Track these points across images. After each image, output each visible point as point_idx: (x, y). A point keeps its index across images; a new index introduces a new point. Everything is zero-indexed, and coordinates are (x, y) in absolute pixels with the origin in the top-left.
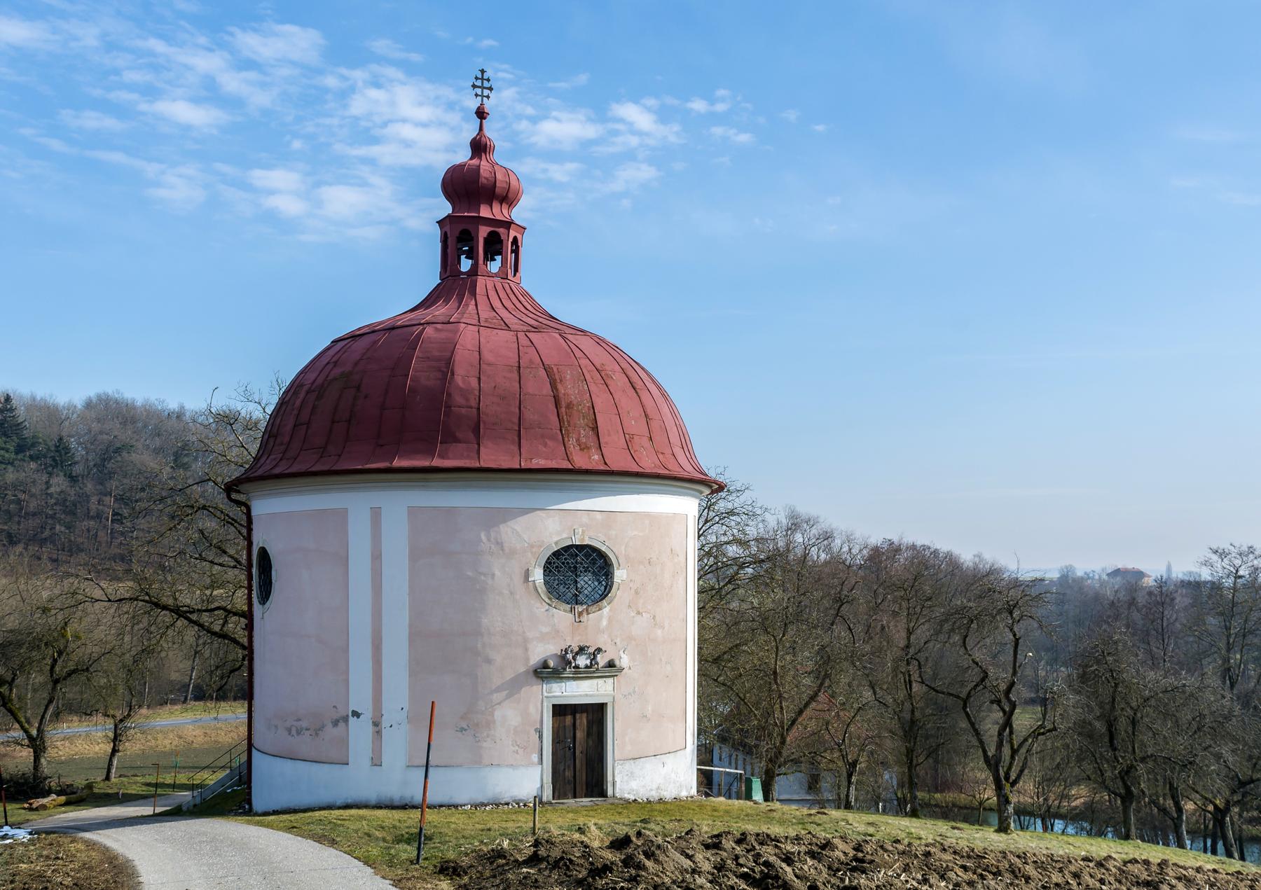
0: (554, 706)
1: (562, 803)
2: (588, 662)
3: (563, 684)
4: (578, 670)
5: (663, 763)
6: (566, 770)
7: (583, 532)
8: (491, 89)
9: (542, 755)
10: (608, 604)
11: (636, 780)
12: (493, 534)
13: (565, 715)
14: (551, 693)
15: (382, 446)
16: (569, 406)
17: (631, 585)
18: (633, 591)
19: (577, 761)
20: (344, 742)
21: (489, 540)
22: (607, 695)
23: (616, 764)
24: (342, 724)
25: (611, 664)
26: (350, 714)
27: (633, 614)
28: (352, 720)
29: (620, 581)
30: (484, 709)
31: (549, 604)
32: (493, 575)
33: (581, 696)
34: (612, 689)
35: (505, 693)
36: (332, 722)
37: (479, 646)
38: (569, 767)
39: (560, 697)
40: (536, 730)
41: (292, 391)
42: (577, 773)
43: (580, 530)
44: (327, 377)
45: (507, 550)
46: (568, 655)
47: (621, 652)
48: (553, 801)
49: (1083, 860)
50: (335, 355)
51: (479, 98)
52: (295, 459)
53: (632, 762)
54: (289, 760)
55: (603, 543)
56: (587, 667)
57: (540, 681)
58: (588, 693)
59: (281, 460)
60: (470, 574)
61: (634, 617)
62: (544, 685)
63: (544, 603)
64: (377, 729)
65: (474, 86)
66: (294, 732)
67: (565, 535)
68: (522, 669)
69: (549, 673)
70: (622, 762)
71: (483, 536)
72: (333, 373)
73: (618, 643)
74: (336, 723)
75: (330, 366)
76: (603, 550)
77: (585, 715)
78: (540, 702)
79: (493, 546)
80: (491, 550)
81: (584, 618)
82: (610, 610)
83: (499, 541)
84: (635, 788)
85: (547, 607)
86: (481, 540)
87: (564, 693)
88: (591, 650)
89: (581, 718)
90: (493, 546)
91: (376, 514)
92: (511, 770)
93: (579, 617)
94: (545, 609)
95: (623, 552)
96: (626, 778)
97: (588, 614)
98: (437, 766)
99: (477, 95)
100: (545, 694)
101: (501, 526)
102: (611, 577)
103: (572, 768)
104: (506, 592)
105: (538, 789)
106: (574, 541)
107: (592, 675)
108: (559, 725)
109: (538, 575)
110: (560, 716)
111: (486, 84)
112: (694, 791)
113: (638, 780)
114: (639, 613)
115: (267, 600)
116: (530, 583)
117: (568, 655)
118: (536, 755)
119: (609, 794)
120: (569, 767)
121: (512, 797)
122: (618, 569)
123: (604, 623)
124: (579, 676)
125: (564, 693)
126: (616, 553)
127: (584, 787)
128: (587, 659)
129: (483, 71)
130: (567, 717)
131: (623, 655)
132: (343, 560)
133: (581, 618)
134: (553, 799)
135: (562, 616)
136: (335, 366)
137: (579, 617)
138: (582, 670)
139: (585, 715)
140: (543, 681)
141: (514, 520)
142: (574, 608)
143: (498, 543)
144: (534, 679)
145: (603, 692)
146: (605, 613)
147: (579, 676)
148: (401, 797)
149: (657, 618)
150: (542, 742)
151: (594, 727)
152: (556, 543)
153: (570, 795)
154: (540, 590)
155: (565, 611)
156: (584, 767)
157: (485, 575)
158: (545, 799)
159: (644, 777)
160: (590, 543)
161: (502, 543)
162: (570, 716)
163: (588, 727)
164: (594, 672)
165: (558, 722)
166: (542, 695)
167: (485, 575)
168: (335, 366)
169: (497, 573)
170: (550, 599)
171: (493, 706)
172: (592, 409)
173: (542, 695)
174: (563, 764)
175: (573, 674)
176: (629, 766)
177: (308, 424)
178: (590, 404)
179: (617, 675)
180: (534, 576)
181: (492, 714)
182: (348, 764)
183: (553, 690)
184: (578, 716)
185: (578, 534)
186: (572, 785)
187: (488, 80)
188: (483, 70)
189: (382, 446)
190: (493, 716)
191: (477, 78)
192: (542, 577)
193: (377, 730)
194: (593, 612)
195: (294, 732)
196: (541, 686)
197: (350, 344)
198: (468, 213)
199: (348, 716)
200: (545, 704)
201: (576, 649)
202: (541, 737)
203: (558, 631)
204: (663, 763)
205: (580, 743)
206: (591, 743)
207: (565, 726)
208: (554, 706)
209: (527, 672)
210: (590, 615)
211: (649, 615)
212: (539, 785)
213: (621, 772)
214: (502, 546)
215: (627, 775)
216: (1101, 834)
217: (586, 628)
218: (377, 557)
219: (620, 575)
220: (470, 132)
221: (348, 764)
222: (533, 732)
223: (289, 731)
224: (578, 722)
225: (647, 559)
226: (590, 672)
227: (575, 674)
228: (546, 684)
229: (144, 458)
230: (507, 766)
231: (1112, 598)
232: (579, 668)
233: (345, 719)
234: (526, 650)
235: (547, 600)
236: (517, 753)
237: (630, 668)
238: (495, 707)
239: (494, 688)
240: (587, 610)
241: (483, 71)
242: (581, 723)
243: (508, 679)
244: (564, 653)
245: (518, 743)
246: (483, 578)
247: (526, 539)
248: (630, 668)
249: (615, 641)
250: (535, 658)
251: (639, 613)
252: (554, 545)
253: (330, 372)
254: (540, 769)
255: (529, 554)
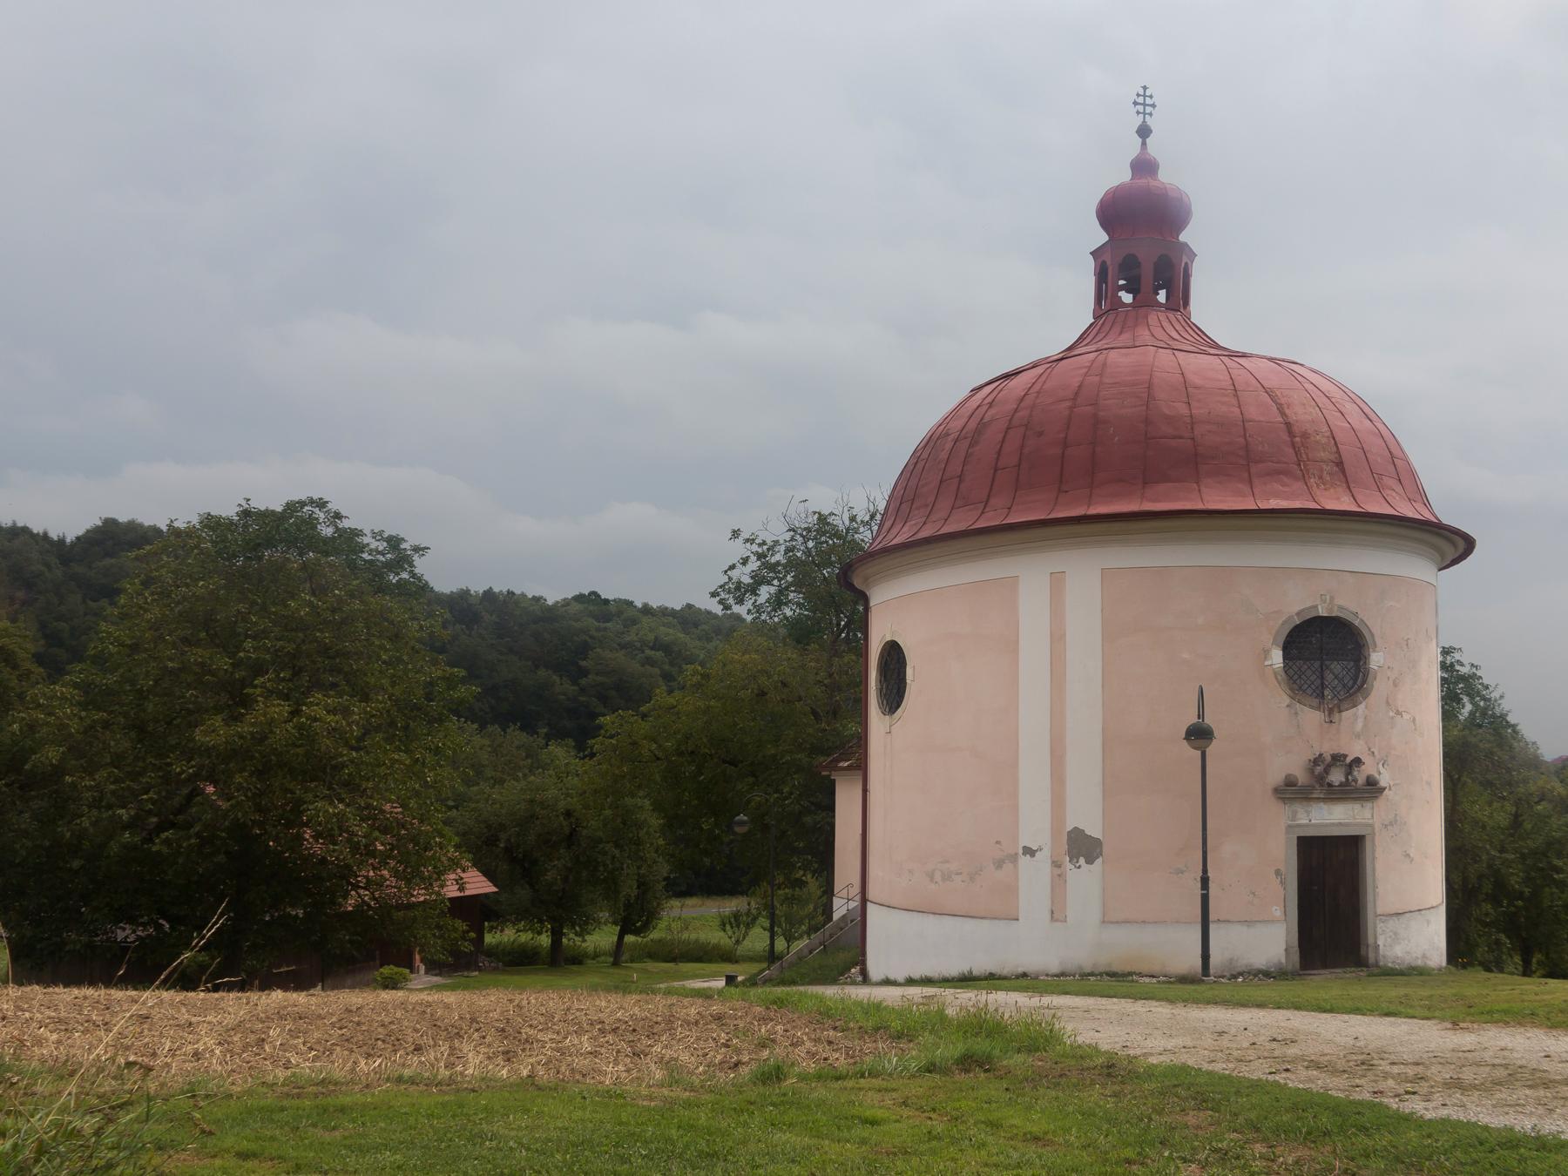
8: (1153, 106)
15: (1066, 492)
16: (1305, 435)
17: (1389, 673)
18: (1391, 682)
20: (1011, 890)
24: (1008, 866)
25: (1371, 783)
26: (1021, 851)
28: (1024, 861)
36: (994, 864)
41: (931, 444)
44: (982, 419)
48: (1301, 972)
49: (1453, 1050)
50: (988, 395)
51: (1141, 116)
52: (946, 520)
54: (932, 916)
56: (1341, 785)
59: (925, 523)
64: (1058, 871)
65: (1135, 103)
66: (938, 876)
72: (989, 413)
73: (1376, 753)
74: (999, 864)
75: (985, 408)
81: (1336, 716)
84: (1400, 955)
87: (1313, 821)
88: (1348, 760)
91: (1057, 580)
94: (1286, 704)
97: (1340, 712)
98: (1144, 922)
99: (1138, 113)
102: (1365, 663)
109: (1277, 657)
111: (1140, 108)
112: (1444, 964)
115: (898, 706)
122: (1374, 651)
123: (1359, 725)
125: (1313, 821)
129: (1145, 88)
132: (1011, 646)
135: (1311, 717)
136: (990, 407)
148: (1231, 959)
149: (1417, 722)
152: (1298, 614)
168: (990, 407)
172: (1331, 439)
176: (1392, 924)
177: (961, 478)
178: (1329, 433)
182: (1017, 920)
187: (1151, 97)
188: (1145, 86)
189: (1066, 492)
191: (1138, 95)
192: (1281, 660)
193: (1059, 873)
195: (938, 876)
197: (1001, 386)
198: (288, 967)
199: (1016, 854)
210: (1344, 714)
216: (49, 986)
218: (1057, 638)
220: (1133, 147)
221: (1017, 920)
223: (931, 877)
226: (1345, 793)
233: (1014, 858)
240: (1339, 707)
241: (1145, 88)
250: (1276, 777)
253: (985, 414)
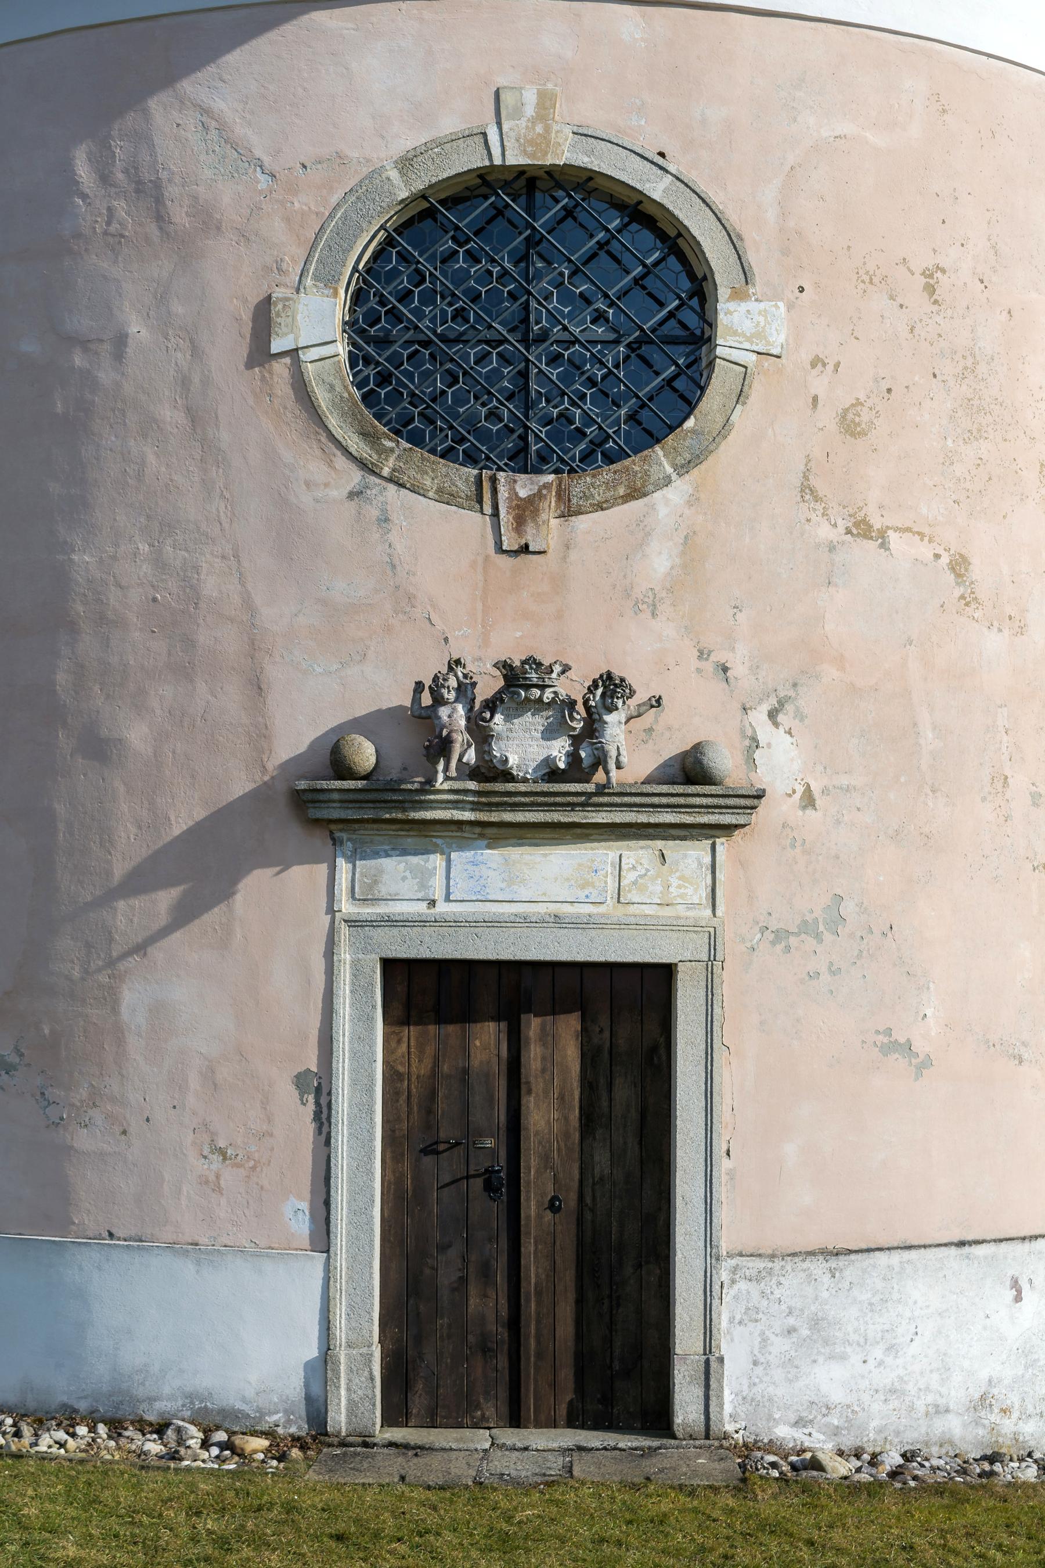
0: (389, 965)
1: (419, 1450)
2: (559, 750)
3: (437, 861)
4: (499, 787)
5: (1015, 1284)
6: (473, 1290)
7: (546, 102)
9: (327, 1203)
10: (683, 469)
11: (843, 1357)
12: (120, 149)
13: (467, 1015)
14: (376, 900)
17: (819, 384)
18: (827, 417)
19: (529, 1248)
21: (105, 178)
22: (675, 926)
23: (724, 1276)
27: (824, 532)
29: (750, 359)
30: (76, 974)
31: (363, 464)
32: (121, 340)
33: (526, 920)
34: (704, 893)
35: (165, 899)
37: (62, 678)
38: (486, 1273)
39: (422, 922)
40: (301, 1081)
42: (531, 1307)
43: (530, 97)
45: (180, 216)
46: (444, 712)
47: (759, 717)
53: (818, 1267)
55: (659, 162)
57: (319, 840)
58: (567, 909)
60: (29, 347)
61: (832, 548)
62: (343, 866)
63: (341, 461)
67: (449, 124)
68: (241, 785)
69: (350, 799)
70: (760, 1264)
71: (84, 172)
73: (739, 670)
76: (656, 196)
77: (569, 1026)
78: (320, 947)
79: (120, 206)
80: (114, 227)
82: (693, 501)
83: (147, 176)
84: (837, 1396)
85: (355, 476)
86: (71, 183)
89: (548, 1038)
90: (120, 206)
92: (187, 1268)
93: (520, 523)
95: (771, 215)
96: (780, 1345)
97: (568, 512)
100: (346, 907)
101: (153, 104)
103: (501, 1279)
104: (171, 415)
105: (309, 1366)
106: (496, 151)
107: (576, 817)
108: (434, 1073)
110: (441, 1020)
113: (855, 1359)
114: (861, 529)
116: (281, 368)
117: (444, 712)
118: (305, 1206)
119: (678, 1420)
120: (486, 1273)
121: (190, 1397)
122: (738, 295)
124: (508, 817)
125: (442, 907)
126: (733, 217)
127: (567, 1375)
128: (549, 734)
130: (476, 1027)
131: (765, 731)
133: (530, 529)
134: (390, 1419)
137: (520, 523)
138: (522, 787)
139: (569, 1026)
140: (335, 841)
141: (211, 69)
142: (494, 480)
143: (140, 186)
144: (295, 832)
145: (648, 910)
146: (662, 511)
147: (508, 817)
149: (976, 571)
150: (328, 1142)
151: (618, 1082)
152: (406, 163)
153: (490, 1411)
154: (322, 398)
155: (446, 497)
156: (569, 1277)
157: (85, 344)
158: (339, 1419)
159: (891, 1349)
160: (582, 160)
161: (157, 184)
162: (492, 1026)
163: (588, 1085)
164: (587, 802)
165: (430, 1050)
166: (331, 910)
167: (85, 344)
169: (138, 329)
170: (368, 436)
171: (111, 963)
173: (331, 910)
174: (453, 1253)
175: (476, 807)
179: (728, 829)
180: (293, 327)
181: (111, 999)
183: (383, 890)
184: (533, 1025)
185: (518, 112)
186: (503, 1362)
190: (115, 1010)
194: (600, 507)
196: (323, 868)
200: (345, 956)
201: (488, 685)
202: (323, 1118)
203: (411, 598)
204: (1015, 1284)
205: (546, 1159)
206: (602, 1159)
207: (466, 1071)
208: (389, 965)
209: (259, 797)
210: (583, 523)
211: (926, 551)
212: (312, 1351)
213: (752, 1315)
214: (159, 200)
215: (791, 1331)
217: (559, 582)
219: (748, 327)
222: (286, 1092)
224: (533, 1056)
225: (917, 266)
227: (490, 807)
228: (352, 859)
229: (570, 760)
230: (170, 1246)
231: (167, 1390)
232: (507, 776)
234: (257, 687)
235: (355, 444)
236: (218, 1189)
237: (809, 800)
238: (122, 966)
239: (120, 869)
242: (549, 1060)
243: (178, 829)
244: (426, 700)
245: (222, 1144)
246: (79, 360)
247: (258, 153)
248: (809, 800)
249: (720, 656)
251: (861, 529)
252: (394, 174)
254: (319, 1273)
255: (278, 224)
